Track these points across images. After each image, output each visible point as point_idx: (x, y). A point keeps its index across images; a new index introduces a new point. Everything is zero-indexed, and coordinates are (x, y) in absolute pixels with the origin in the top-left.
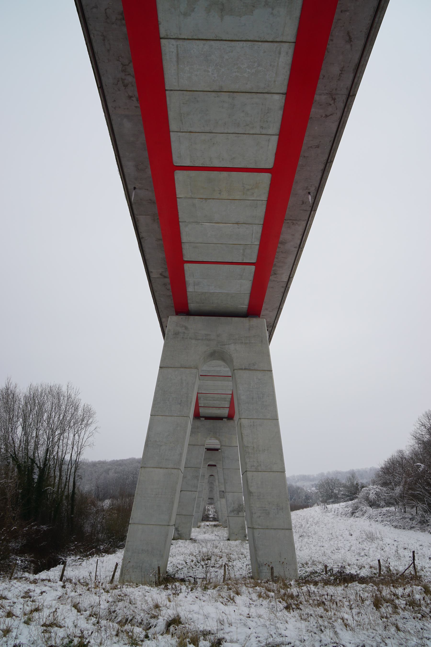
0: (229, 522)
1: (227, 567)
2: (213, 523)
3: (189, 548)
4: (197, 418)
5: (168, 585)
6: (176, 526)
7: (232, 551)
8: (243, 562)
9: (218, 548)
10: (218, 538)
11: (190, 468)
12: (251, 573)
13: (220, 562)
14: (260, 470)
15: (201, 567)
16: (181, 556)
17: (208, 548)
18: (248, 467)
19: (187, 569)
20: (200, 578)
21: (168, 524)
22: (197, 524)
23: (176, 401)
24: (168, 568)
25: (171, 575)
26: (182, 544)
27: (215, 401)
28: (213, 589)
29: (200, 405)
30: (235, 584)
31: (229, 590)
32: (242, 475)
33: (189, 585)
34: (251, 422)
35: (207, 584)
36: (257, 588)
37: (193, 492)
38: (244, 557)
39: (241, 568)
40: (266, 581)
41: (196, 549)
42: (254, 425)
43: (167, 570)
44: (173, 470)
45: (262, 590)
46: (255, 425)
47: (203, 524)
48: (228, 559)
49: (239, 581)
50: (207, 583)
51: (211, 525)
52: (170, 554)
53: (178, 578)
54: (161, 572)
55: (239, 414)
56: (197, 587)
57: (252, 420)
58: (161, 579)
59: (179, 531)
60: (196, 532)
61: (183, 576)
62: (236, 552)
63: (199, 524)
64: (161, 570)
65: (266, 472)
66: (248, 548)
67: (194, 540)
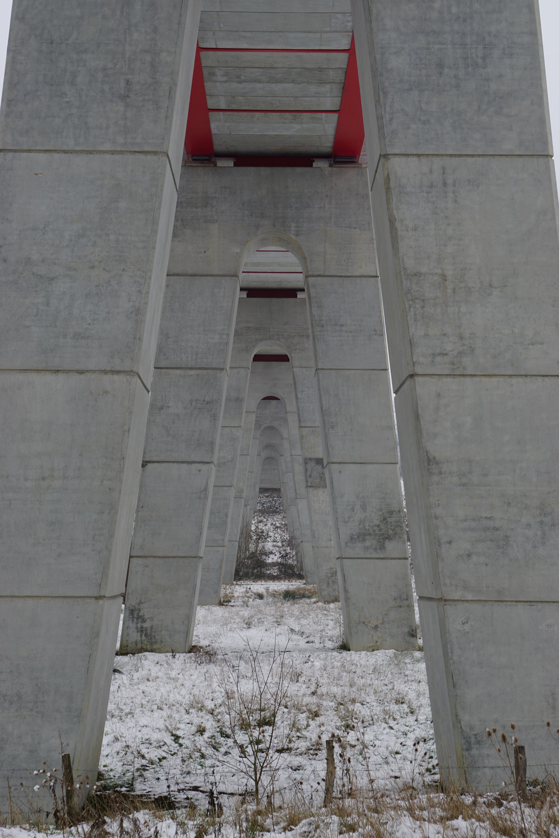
0: (344, 581)
1: (337, 749)
2: (283, 586)
3: (188, 684)
4: (202, 161)
5: (104, 822)
6: (132, 601)
7: (360, 690)
8: (404, 729)
9: (301, 680)
10: (302, 643)
11: (178, 372)
12: (437, 770)
13: (312, 734)
14: (469, 372)
15: (236, 752)
16: (157, 714)
17: (261, 679)
18: (422, 359)
19: (179, 761)
20: (232, 794)
21: (96, 594)
22: (217, 592)
23: (106, 87)
24: (103, 761)
25: (117, 786)
26: (158, 667)
27: (277, 81)
28: (285, 829)
29: (211, 103)
30: (369, 809)
31: (348, 831)
32: (395, 392)
33: (191, 817)
34: (431, 172)
35: (259, 813)
36: (460, 823)
37: (194, 466)
38: (407, 710)
39: (397, 753)
40: (495, 799)
41: (215, 685)
42: (445, 184)
43: (101, 768)
44: (107, 378)
45: (478, 832)
46: (450, 181)
47: (239, 590)
48: (342, 718)
49: (388, 800)
50: (262, 807)
51: (274, 595)
52: (111, 707)
53: (147, 796)
54: (75, 774)
55: (382, 136)
56: (221, 825)
57: (438, 163)
58: (77, 801)
59: (144, 621)
60: (215, 621)
61: (165, 789)
62: (375, 692)
63: (225, 590)
64: (74, 767)
65: (495, 379)
66: (423, 677)
67: (207, 653)
